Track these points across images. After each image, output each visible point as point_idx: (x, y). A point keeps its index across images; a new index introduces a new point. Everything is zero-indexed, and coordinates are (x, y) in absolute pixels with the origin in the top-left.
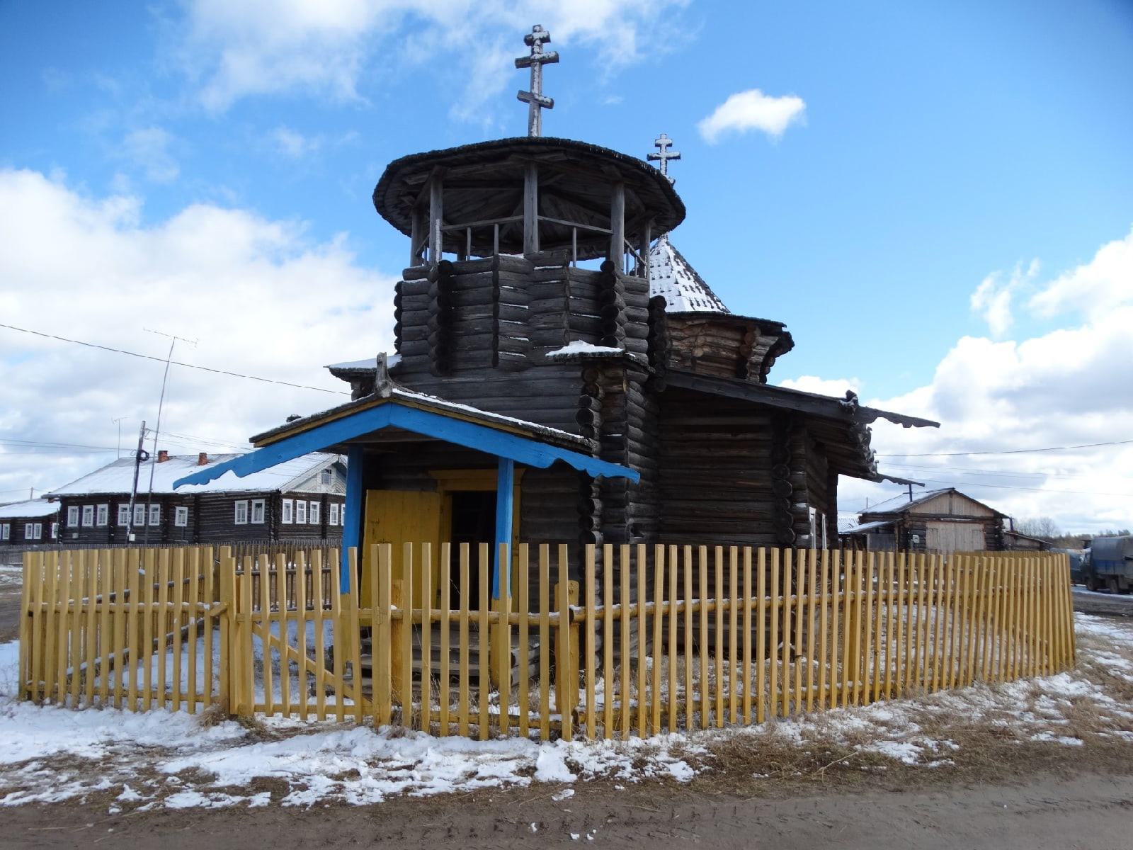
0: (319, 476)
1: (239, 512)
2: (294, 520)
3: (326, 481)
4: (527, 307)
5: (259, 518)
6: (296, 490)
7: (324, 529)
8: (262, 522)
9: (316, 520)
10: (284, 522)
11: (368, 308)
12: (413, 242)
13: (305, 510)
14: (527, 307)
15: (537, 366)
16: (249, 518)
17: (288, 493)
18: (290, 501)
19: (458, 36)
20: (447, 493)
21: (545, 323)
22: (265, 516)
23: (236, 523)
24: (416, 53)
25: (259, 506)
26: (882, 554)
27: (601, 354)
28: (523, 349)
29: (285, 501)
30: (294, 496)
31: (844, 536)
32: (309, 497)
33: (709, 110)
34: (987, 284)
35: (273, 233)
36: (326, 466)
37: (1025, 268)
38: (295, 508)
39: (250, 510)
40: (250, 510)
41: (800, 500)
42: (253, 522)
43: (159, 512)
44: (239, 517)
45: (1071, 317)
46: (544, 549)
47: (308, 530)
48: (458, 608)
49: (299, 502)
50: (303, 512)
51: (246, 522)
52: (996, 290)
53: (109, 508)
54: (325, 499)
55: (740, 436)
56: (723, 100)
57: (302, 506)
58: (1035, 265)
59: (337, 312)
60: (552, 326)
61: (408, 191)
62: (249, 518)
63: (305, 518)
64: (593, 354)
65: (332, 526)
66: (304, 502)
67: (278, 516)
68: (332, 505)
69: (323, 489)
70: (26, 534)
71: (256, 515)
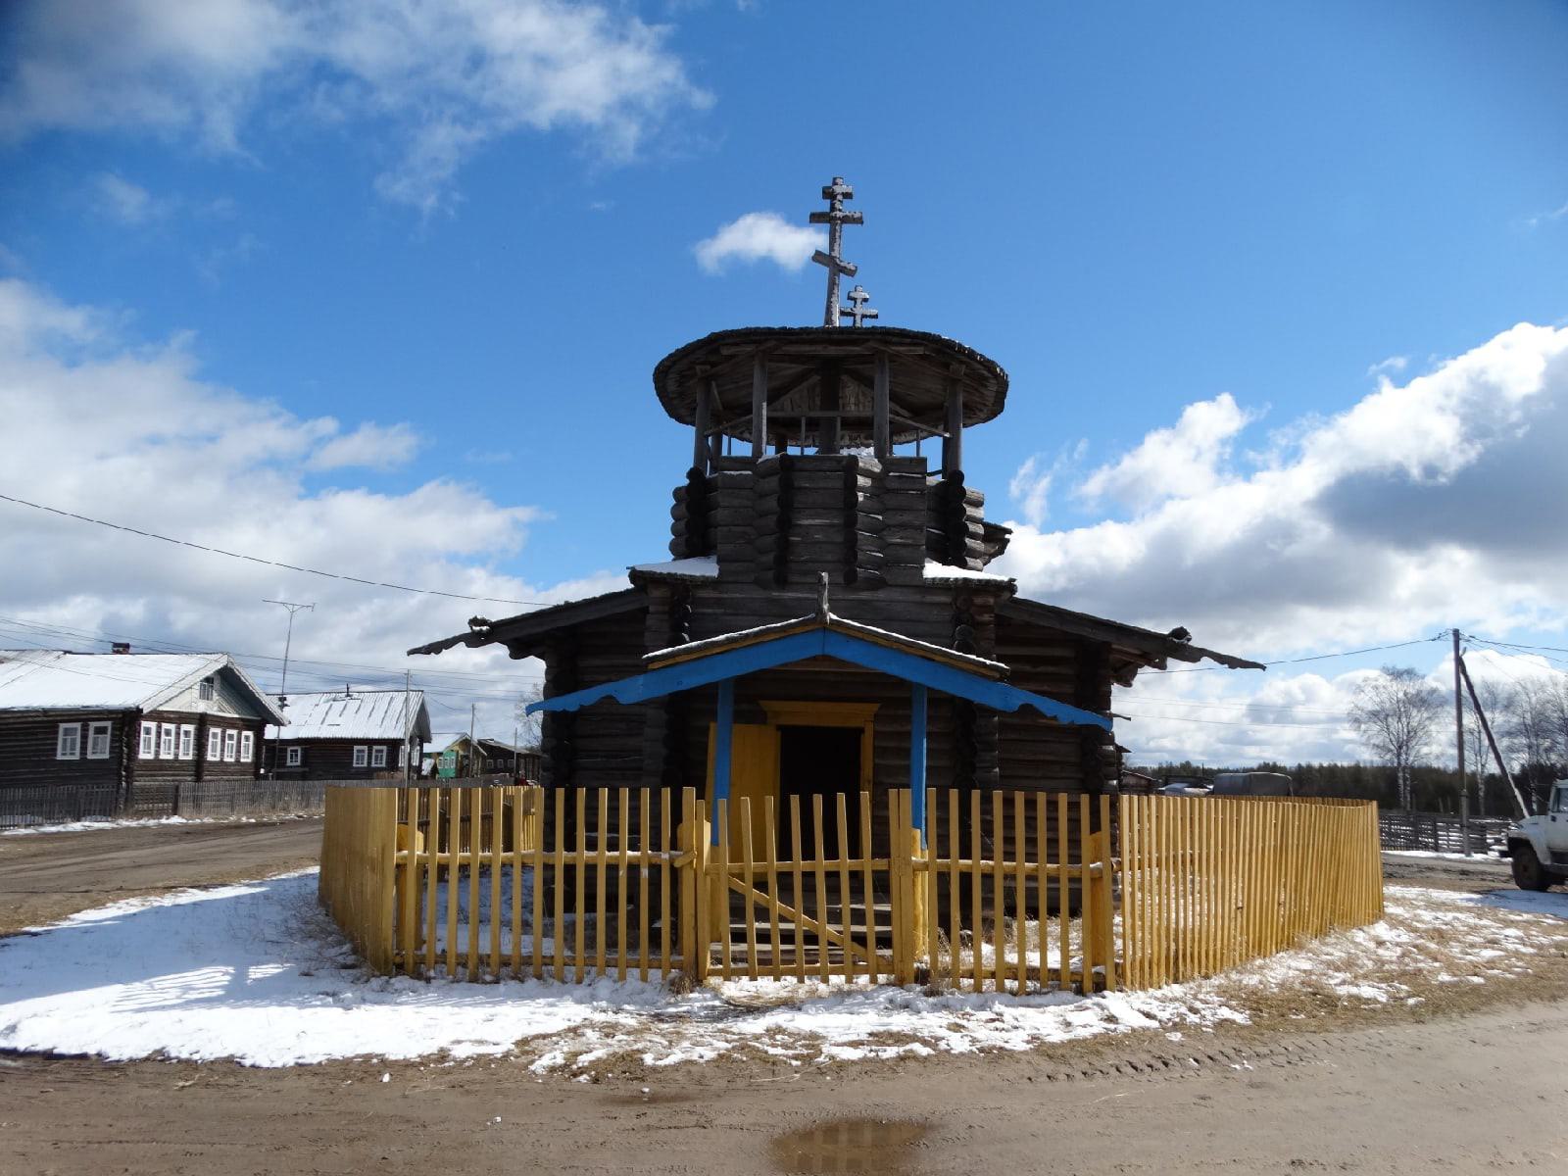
0: (197, 687)
1: (65, 741)
2: (177, 755)
3: (205, 695)
4: (880, 517)
5: (101, 750)
6: (160, 709)
7: (199, 765)
8: (106, 756)
9: (187, 755)
10: (210, 758)
11: (212, 439)
12: (697, 431)
13: (173, 738)
14: (880, 517)
15: (891, 586)
16: (84, 748)
17: (151, 712)
18: (153, 725)
19: (389, 100)
20: (779, 728)
21: (901, 538)
22: (111, 747)
23: (59, 757)
24: (327, 110)
25: (100, 731)
26: (1243, 802)
27: (966, 580)
28: (878, 564)
29: (145, 724)
30: (159, 716)
31: (639, 790)
32: (180, 718)
33: (712, 233)
34: (1029, 466)
35: (73, 321)
36: (209, 673)
37: (1073, 449)
38: (178, 734)
39: (84, 737)
40: (84, 737)
41: (1106, 742)
42: (90, 756)
43: (108, 736)
44: (64, 748)
45: (1118, 508)
46: (646, 794)
47: (176, 768)
48: (813, 858)
49: (165, 726)
50: (170, 741)
51: (77, 757)
52: (1037, 475)
53: (255, 735)
54: (202, 722)
55: (1040, 669)
56: (732, 218)
57: (168, 733)
58: (1083, 446)
59: (155, 440)
60: (910, 541)
61: (703, 380)
62: (84, 748)
63: (218, 753)
64: (956, 580)
65: (211, 763)
66: (172, 727)
67: (133, 748)
68: (213, 730)
69: (202, 707)
70: (354, 761)
71: (95, 744)
